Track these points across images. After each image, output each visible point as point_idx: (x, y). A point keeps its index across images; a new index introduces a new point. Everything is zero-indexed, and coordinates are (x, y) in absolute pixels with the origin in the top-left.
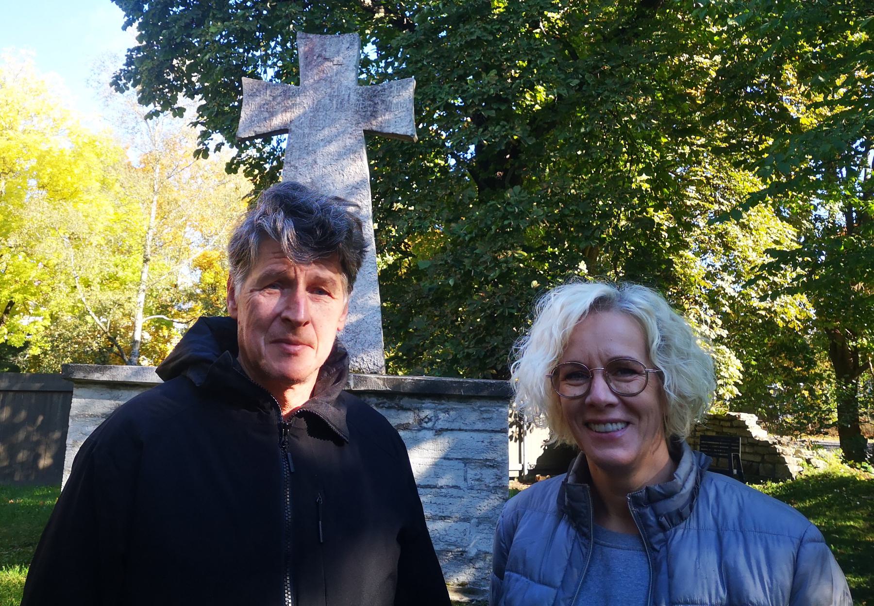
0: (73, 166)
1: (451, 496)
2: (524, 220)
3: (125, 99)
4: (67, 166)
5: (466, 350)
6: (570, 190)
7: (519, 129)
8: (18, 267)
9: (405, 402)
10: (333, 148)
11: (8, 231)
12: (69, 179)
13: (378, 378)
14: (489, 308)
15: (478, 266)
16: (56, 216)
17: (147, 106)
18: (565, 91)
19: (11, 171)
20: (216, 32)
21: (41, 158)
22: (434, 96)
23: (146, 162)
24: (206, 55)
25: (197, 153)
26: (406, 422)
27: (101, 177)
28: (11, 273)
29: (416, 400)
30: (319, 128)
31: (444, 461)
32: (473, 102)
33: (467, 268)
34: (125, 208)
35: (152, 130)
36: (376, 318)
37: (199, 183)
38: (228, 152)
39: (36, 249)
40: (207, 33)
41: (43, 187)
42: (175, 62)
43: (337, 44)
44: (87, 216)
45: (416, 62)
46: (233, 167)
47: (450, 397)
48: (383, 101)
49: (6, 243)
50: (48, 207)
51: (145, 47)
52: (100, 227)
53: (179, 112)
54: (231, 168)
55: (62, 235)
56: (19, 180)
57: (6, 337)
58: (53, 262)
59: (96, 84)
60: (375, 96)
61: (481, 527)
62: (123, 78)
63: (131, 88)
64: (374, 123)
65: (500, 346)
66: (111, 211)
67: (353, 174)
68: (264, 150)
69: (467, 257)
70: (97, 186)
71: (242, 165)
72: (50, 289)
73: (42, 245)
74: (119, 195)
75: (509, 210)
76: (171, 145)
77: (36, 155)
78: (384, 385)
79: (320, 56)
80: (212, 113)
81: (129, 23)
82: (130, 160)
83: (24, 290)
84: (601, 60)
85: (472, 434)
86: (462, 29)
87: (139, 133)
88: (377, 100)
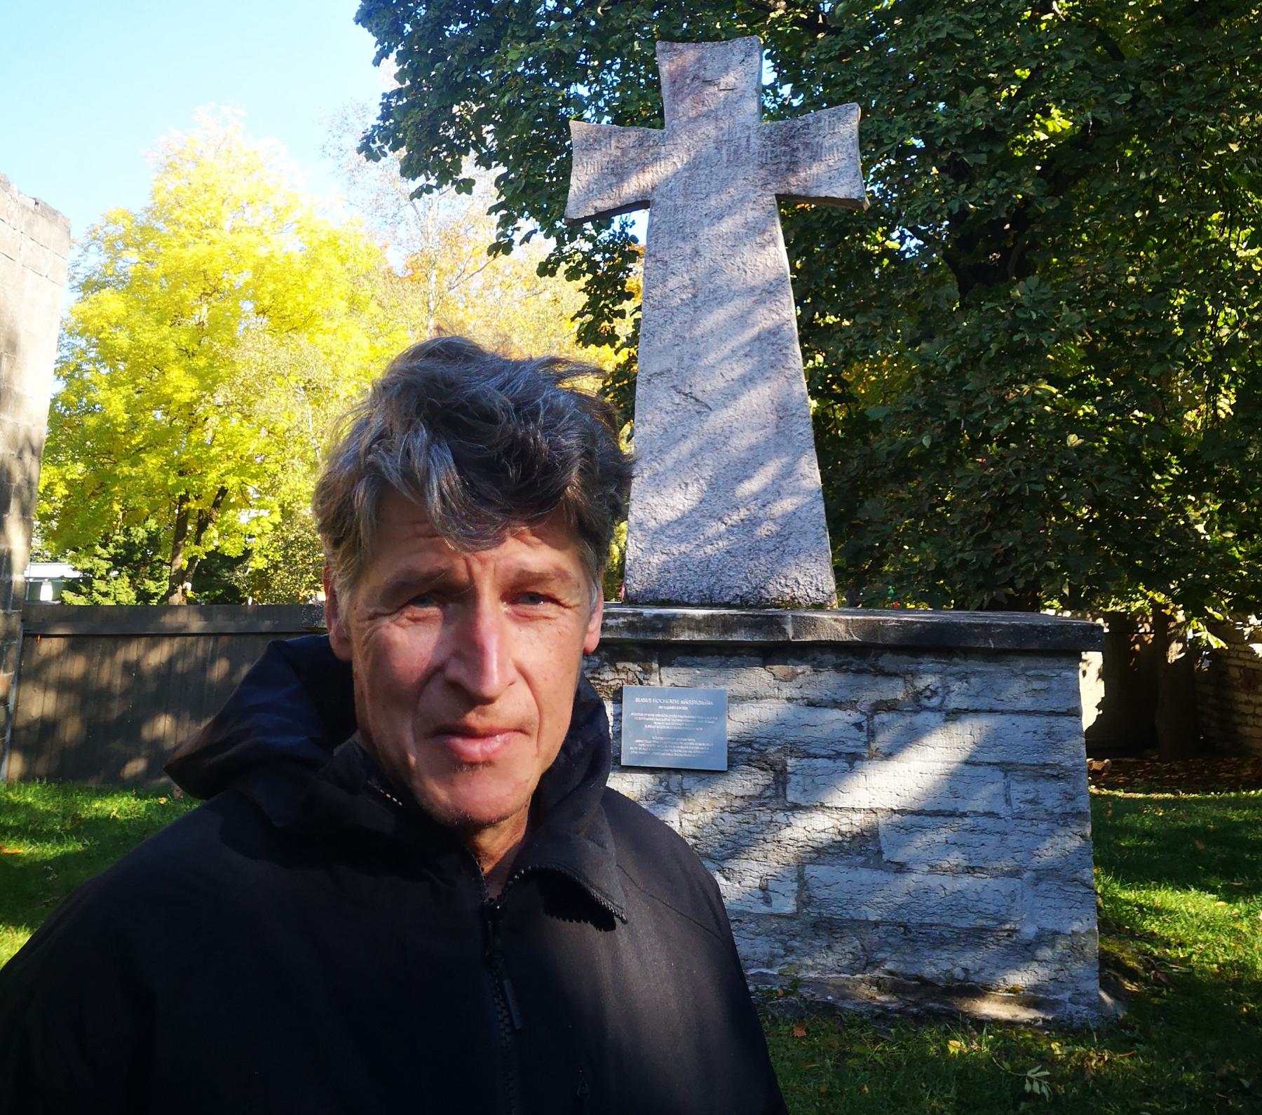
0: (306, 279)
1: (983, 831)
2: (1047, 333)
3: (380, 172)
4: (296, 278)
5: (959, 556)
6: (1127, 277)
7: (1029, 184)
8: (231, 435)
9: (887, 661)
10: (726, 226)
11: (215, 382)
12: (300, 298)
13: (836, 620)
14: (995, 483)
15: (971, 412)
16: (284, 356)
17: (413, 180)
18: (1107, 115)
19: (216, 290)
20: (518, 60)
21: (258, 269)
22: (878, 135)
23: (414, 266)
24: (504, 96)
25: (495, 249)
26: (891, 696)
27: (349, 292)
28: (220, 445)
29: (906, 658)
30: (699, 196)
31: (967, 768)
32: (946, 141)
33: (952, 417)
34: (387, 339)
35: (422, 217)
36: (815, 511)
37: (498, 295)
38: (540, 245)
39: (257, 407)
40: (505, 61)
41: (264, 312)
42: (456, 109)
43: (724, 56)
44: (330, 354)
45: (844, 84)
46: (550, 266)
47: (968, 653)
48: (807, 145)
49: (212, 400)
50: (271, 343)
51: (410, 88)
52: (349, 370)
53: (466, 186)
54: (546, 269)
55: (293, 383)
56: (229, 304)
57: (216, 543)
58: (282, 425)
59: (335, 152)
60: (793, 137)
61: (1043, 886)
62: (377, 138)
63: (390, 154)
64: (793, 180)
65: (1019, 548)
66: (365, 343)
67: (761, 268)
68: (599, 238)
69: (950, 398)
70: (343, 306)
71: (563, 263)
72: (279, 469)
73: (266, 401)
74: (377, 320)
75: (1021, 315)
76: (451, 239)
77: (251, 264)
78: (847, 632)
79: (696, 77)
80: (517, 188)
81: (383, 54)
82: (390, 264)
83: (241, 470)
84: (1168, 55)
85: (1015, 718)
86: (921, 23)
87: (403, 223)
88: (796, 143)
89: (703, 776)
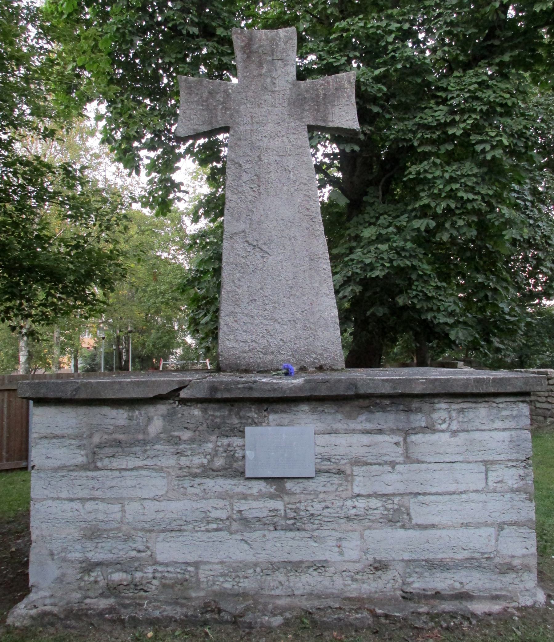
89: (300, 481)
